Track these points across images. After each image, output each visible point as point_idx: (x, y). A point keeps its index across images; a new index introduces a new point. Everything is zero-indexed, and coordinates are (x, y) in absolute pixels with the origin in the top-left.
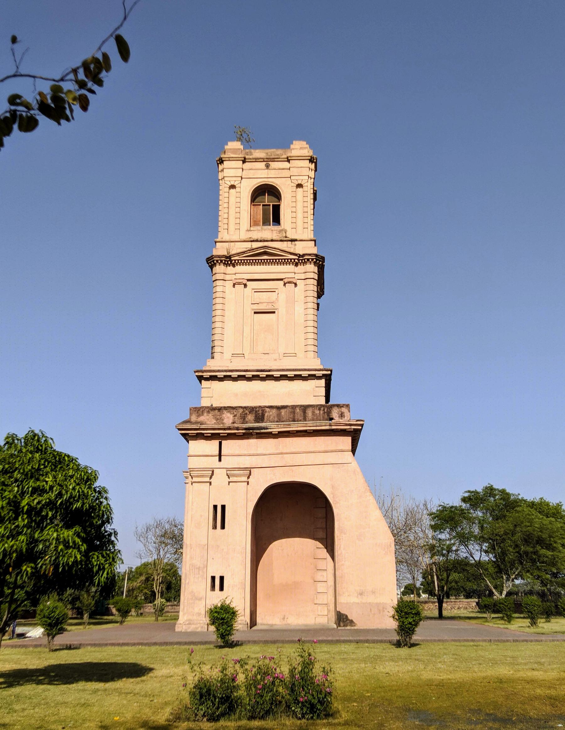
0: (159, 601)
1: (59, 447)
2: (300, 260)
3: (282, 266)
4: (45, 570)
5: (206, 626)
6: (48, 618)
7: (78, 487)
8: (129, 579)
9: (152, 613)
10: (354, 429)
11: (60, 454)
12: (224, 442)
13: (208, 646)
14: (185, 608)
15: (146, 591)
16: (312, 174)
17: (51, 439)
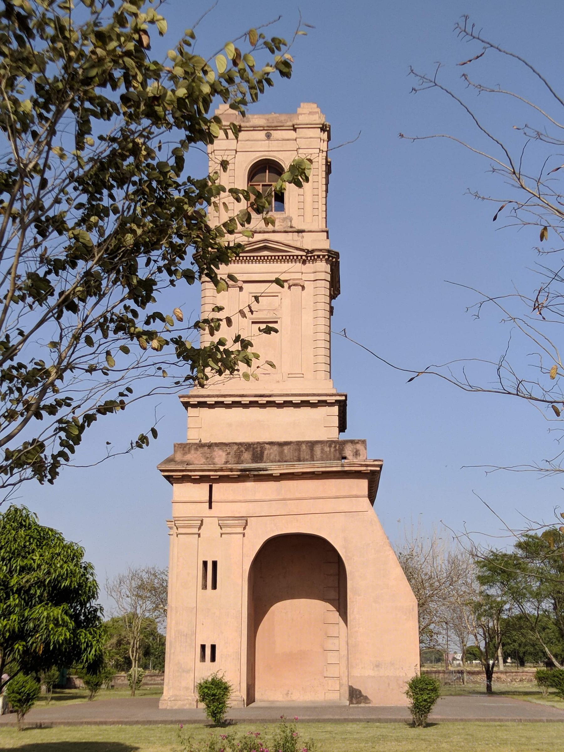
0: (135, 670)
1: (43, 521)
3: (286, 264)
4: (36, 648)
5: (195, 704)
6: (17, 693)
7: (65, 566)
9: (126, 685)
10: (371, 470)
11: (43, 529)
12: (215, 486)
13: (197, 725)
14: (170, 682)
15: (117, 657)
16: (324, 146)
17: (35, 514)
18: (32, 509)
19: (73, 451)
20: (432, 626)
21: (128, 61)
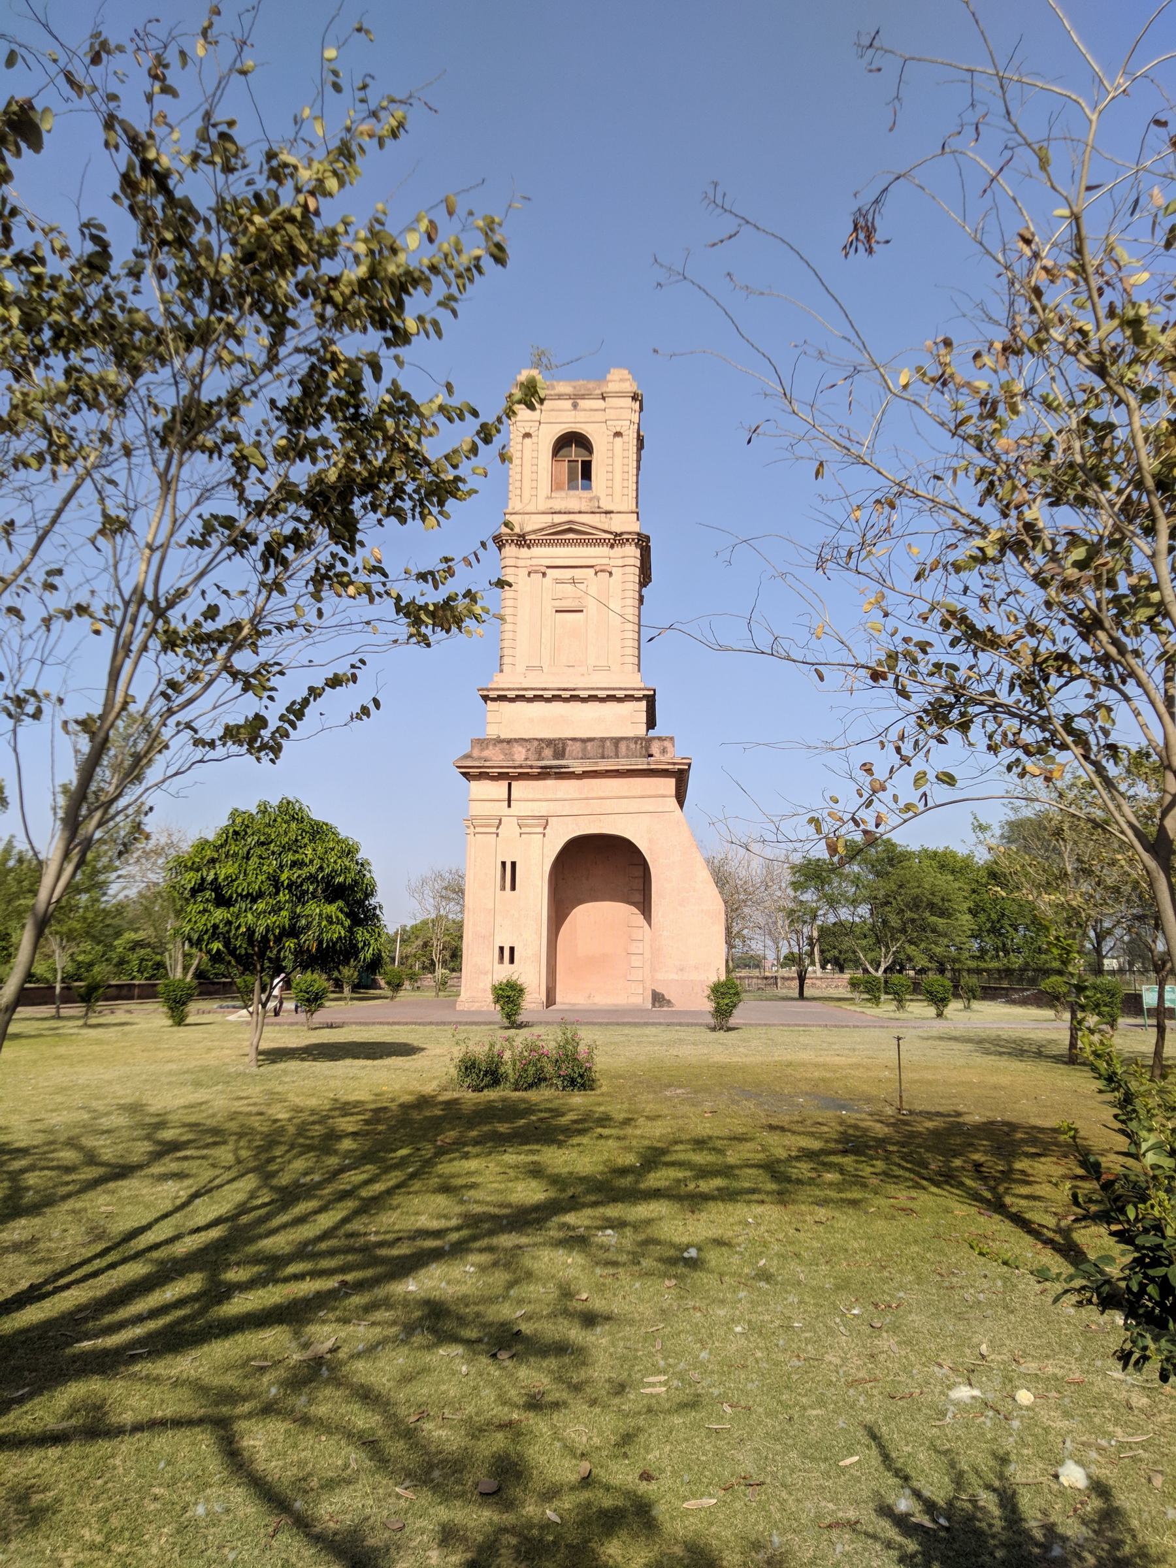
0: (440, 971)
2: (617, 540)
8: (403, 941)
11: (317, 823)
12: (514, 784)
16: (635, 417)
18: (305, 803)
19: (294, 727)
20: (745, 932)
21: (292, 229)
